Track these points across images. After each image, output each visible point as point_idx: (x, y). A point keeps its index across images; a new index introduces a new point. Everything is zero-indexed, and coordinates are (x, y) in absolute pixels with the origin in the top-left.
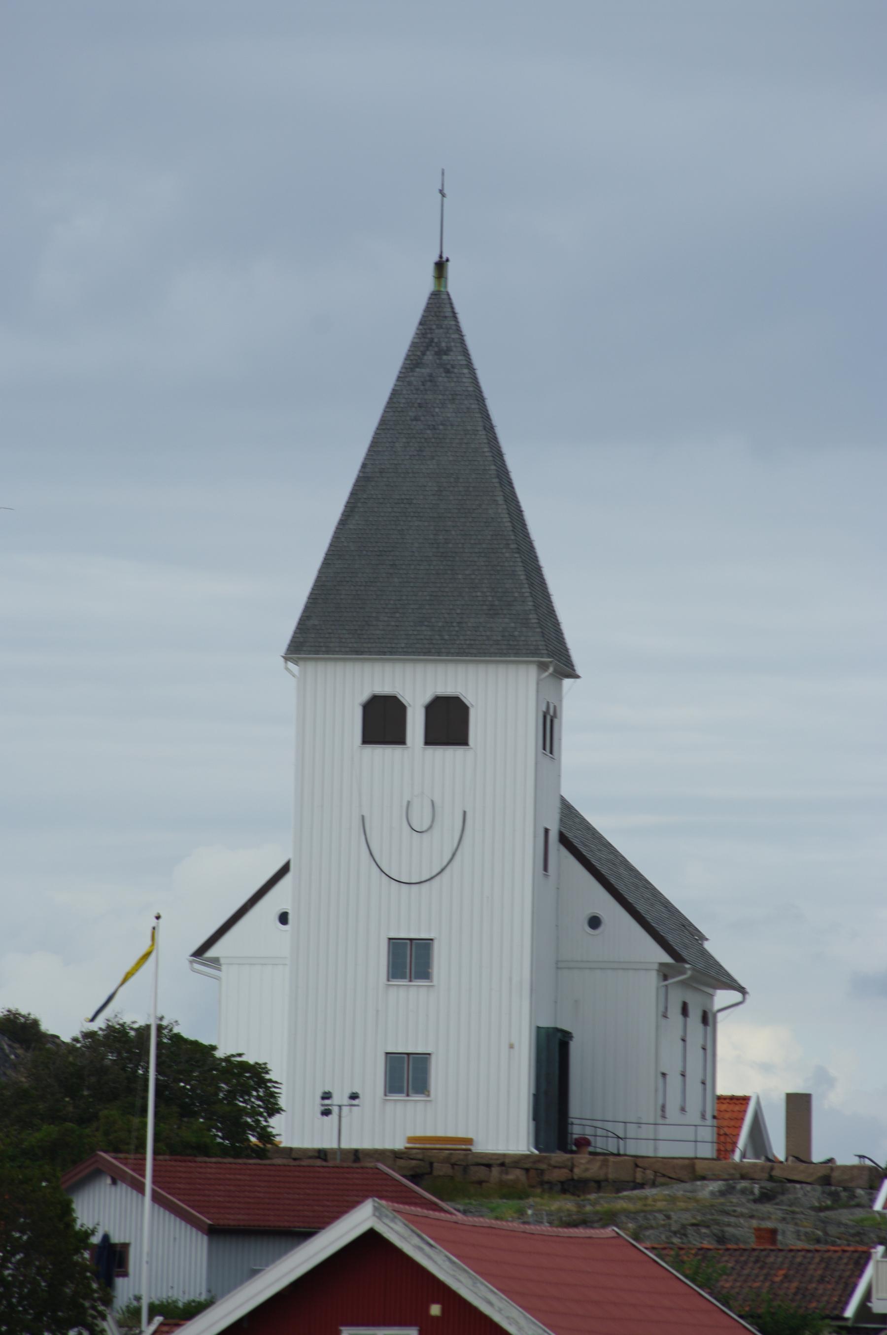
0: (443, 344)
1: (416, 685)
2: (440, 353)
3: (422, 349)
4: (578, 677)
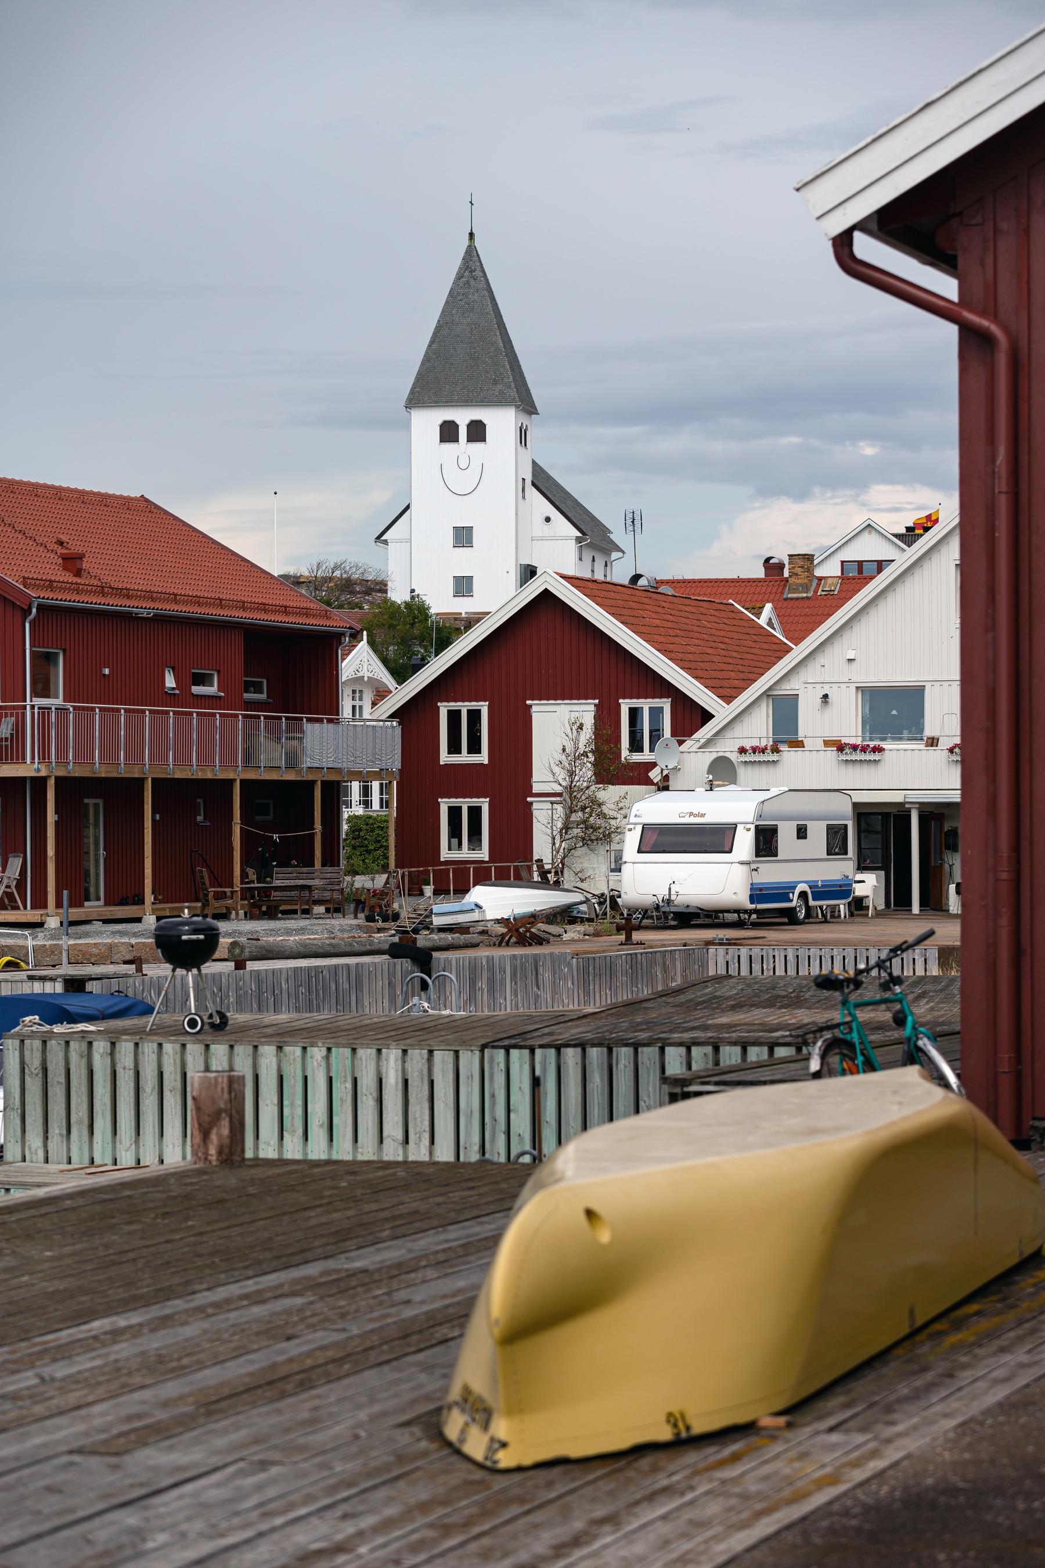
1: (462, 417)
2: (471, 272)
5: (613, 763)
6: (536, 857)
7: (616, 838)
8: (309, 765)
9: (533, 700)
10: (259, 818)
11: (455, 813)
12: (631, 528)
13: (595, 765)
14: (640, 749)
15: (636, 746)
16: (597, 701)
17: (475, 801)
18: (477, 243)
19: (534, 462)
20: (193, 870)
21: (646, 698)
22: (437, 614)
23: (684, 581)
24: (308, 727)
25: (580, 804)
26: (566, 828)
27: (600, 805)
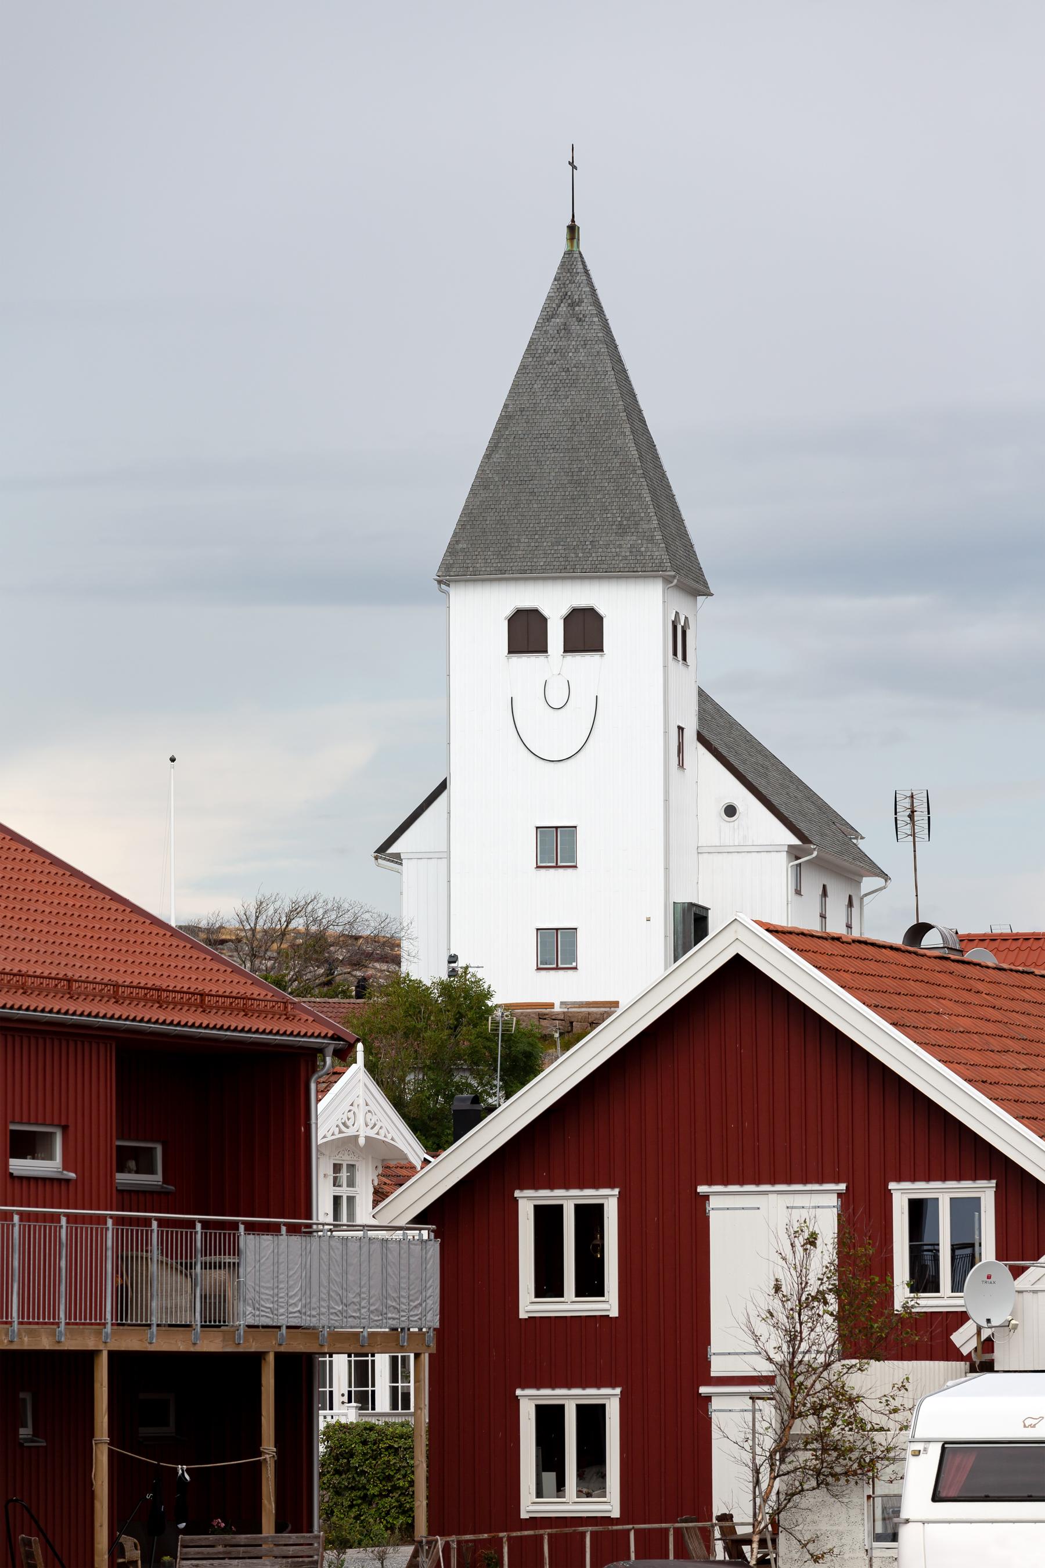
0: (576, 297)
1: (555, 601)
2: (572, 305)
3: (557, 302)
4: (712, 595)
5: (877, 1316)
6: (718, 1509)
7: (886, 1471)
8: (251, 1321)
9: (710, 1183)
10: (145, 1431)
11: (549, 1419)
12: (908, 829)
13: (839, 1318)
14: (933, 1286)
15: (924, 1279)
16: (842, 1187)
17: (591, 1395)
18: (586, 246)
19: (701, 693)
20: (10, 1538)
21: (944, 1179)
22: (508, 1007)
23: (1016, 938)
24: (248, 1242)
25: (810, 1400)
26: (783, 1449)
27: (852, 1401)
